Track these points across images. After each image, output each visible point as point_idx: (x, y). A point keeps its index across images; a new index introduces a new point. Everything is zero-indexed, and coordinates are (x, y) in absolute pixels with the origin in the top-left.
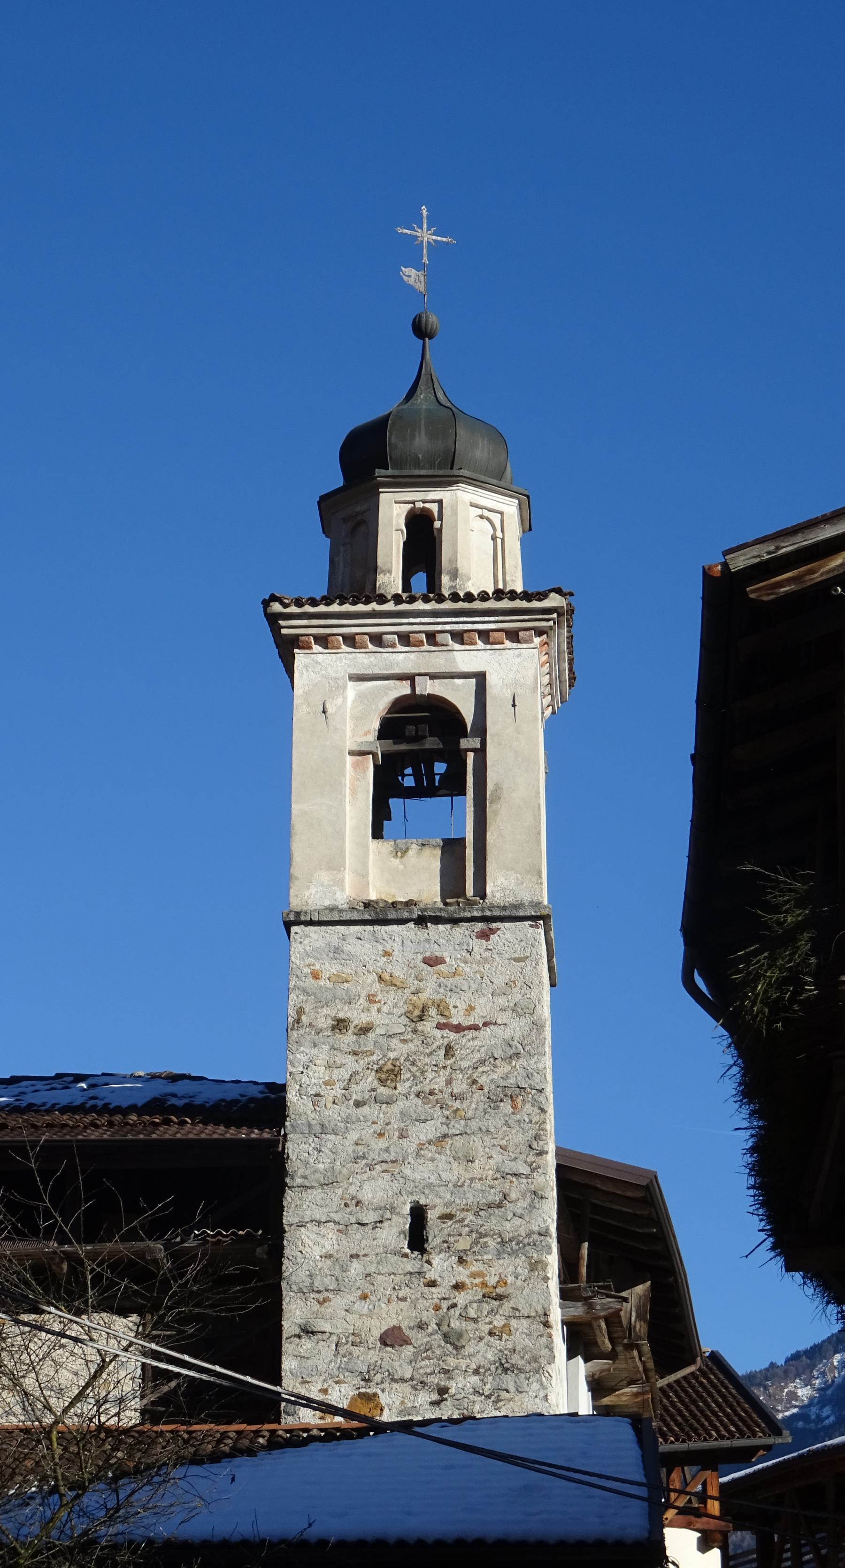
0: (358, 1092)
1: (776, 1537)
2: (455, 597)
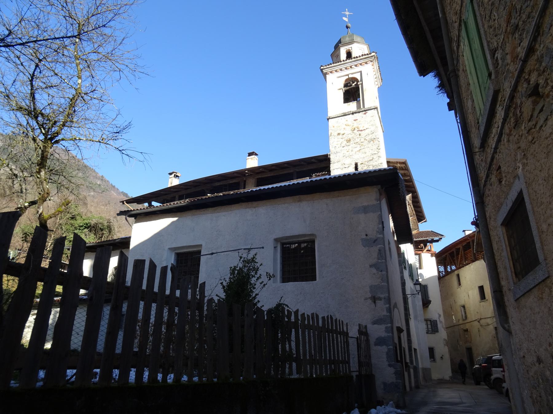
0: (343, 145)
2: (354, 58)
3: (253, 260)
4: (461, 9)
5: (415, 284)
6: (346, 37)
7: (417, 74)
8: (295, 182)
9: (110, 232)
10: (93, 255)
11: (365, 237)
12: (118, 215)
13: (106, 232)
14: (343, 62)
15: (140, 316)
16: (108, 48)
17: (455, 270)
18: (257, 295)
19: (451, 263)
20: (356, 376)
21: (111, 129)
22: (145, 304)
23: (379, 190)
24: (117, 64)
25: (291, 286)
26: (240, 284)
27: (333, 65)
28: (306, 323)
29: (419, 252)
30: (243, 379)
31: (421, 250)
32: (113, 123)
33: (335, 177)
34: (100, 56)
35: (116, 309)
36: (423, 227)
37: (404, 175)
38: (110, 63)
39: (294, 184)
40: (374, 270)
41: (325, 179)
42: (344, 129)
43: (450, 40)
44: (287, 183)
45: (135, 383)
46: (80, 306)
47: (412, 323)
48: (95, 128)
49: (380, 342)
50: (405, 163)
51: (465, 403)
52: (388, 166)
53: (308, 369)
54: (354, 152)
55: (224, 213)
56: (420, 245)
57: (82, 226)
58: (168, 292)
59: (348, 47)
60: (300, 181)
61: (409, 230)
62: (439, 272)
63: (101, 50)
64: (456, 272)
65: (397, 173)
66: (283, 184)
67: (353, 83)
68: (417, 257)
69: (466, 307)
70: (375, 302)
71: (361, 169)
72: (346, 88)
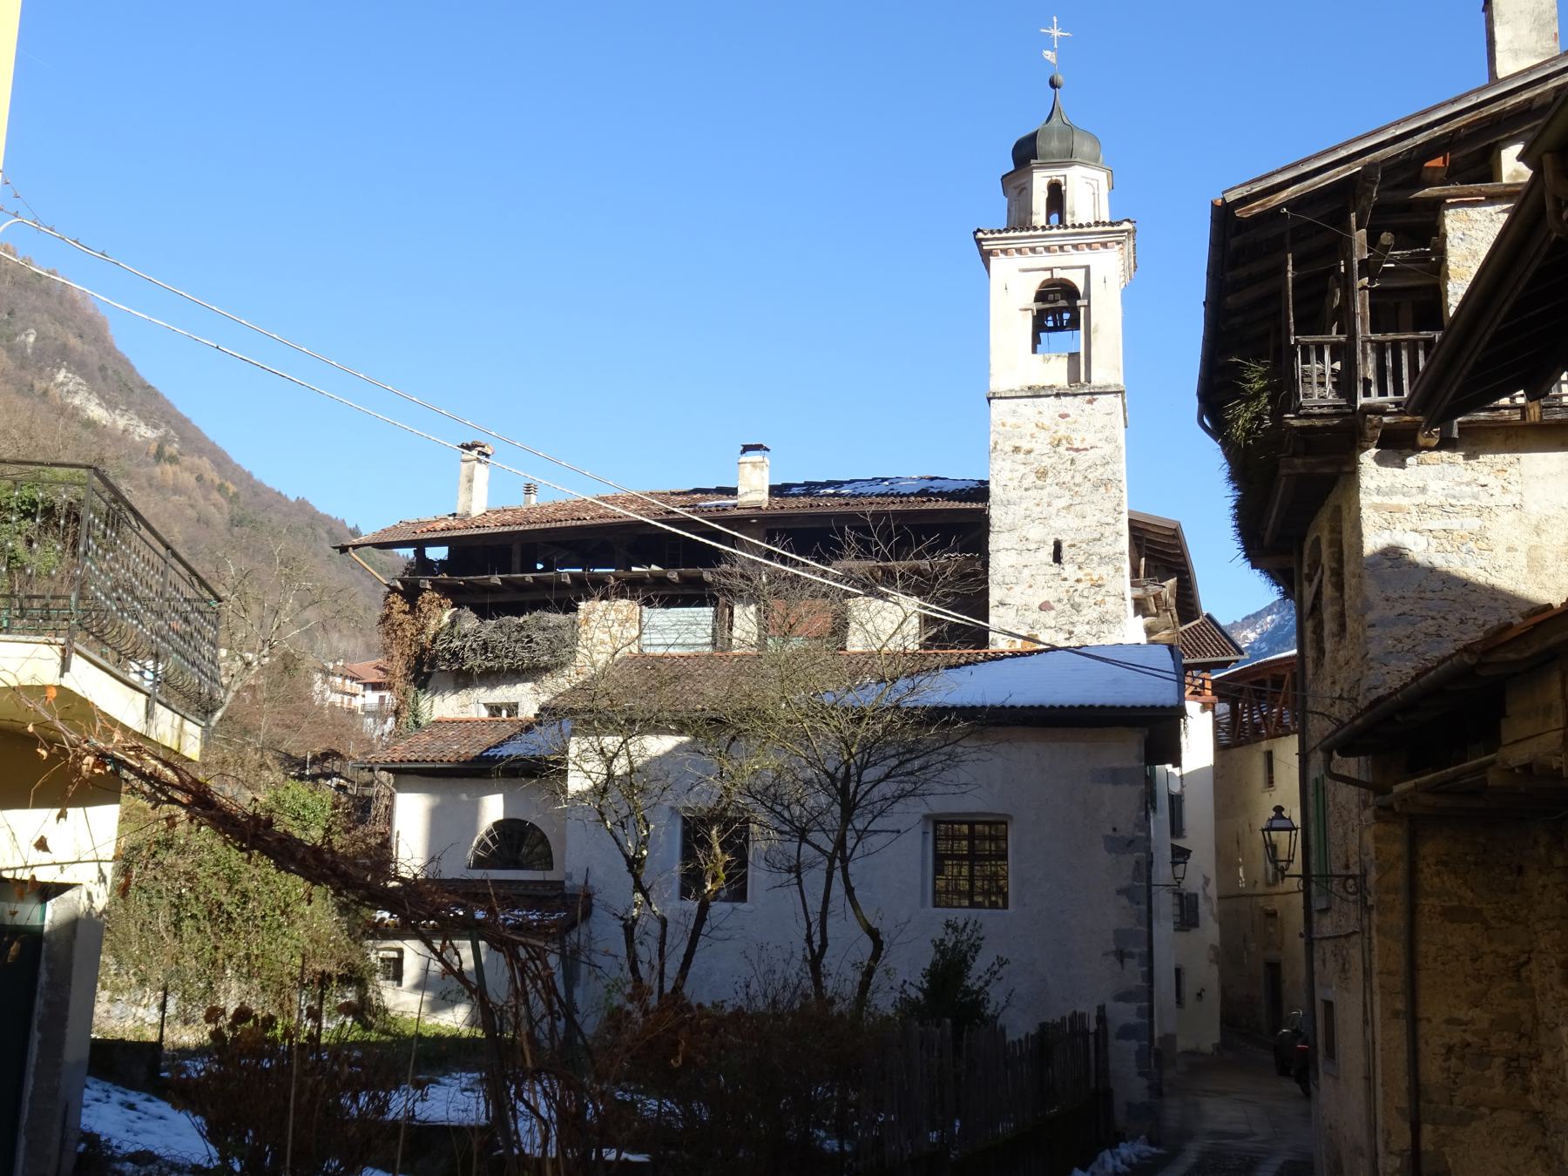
0: (1026, 484)
2: (1074, 226)
11: (1110, 833)
27: (1011, 234)
40: (1124, 901)
42: (1032, 436)
49: (1126, 1032)
54: (1053, 510)
59: (1056, 174)
72: (1041, 305)
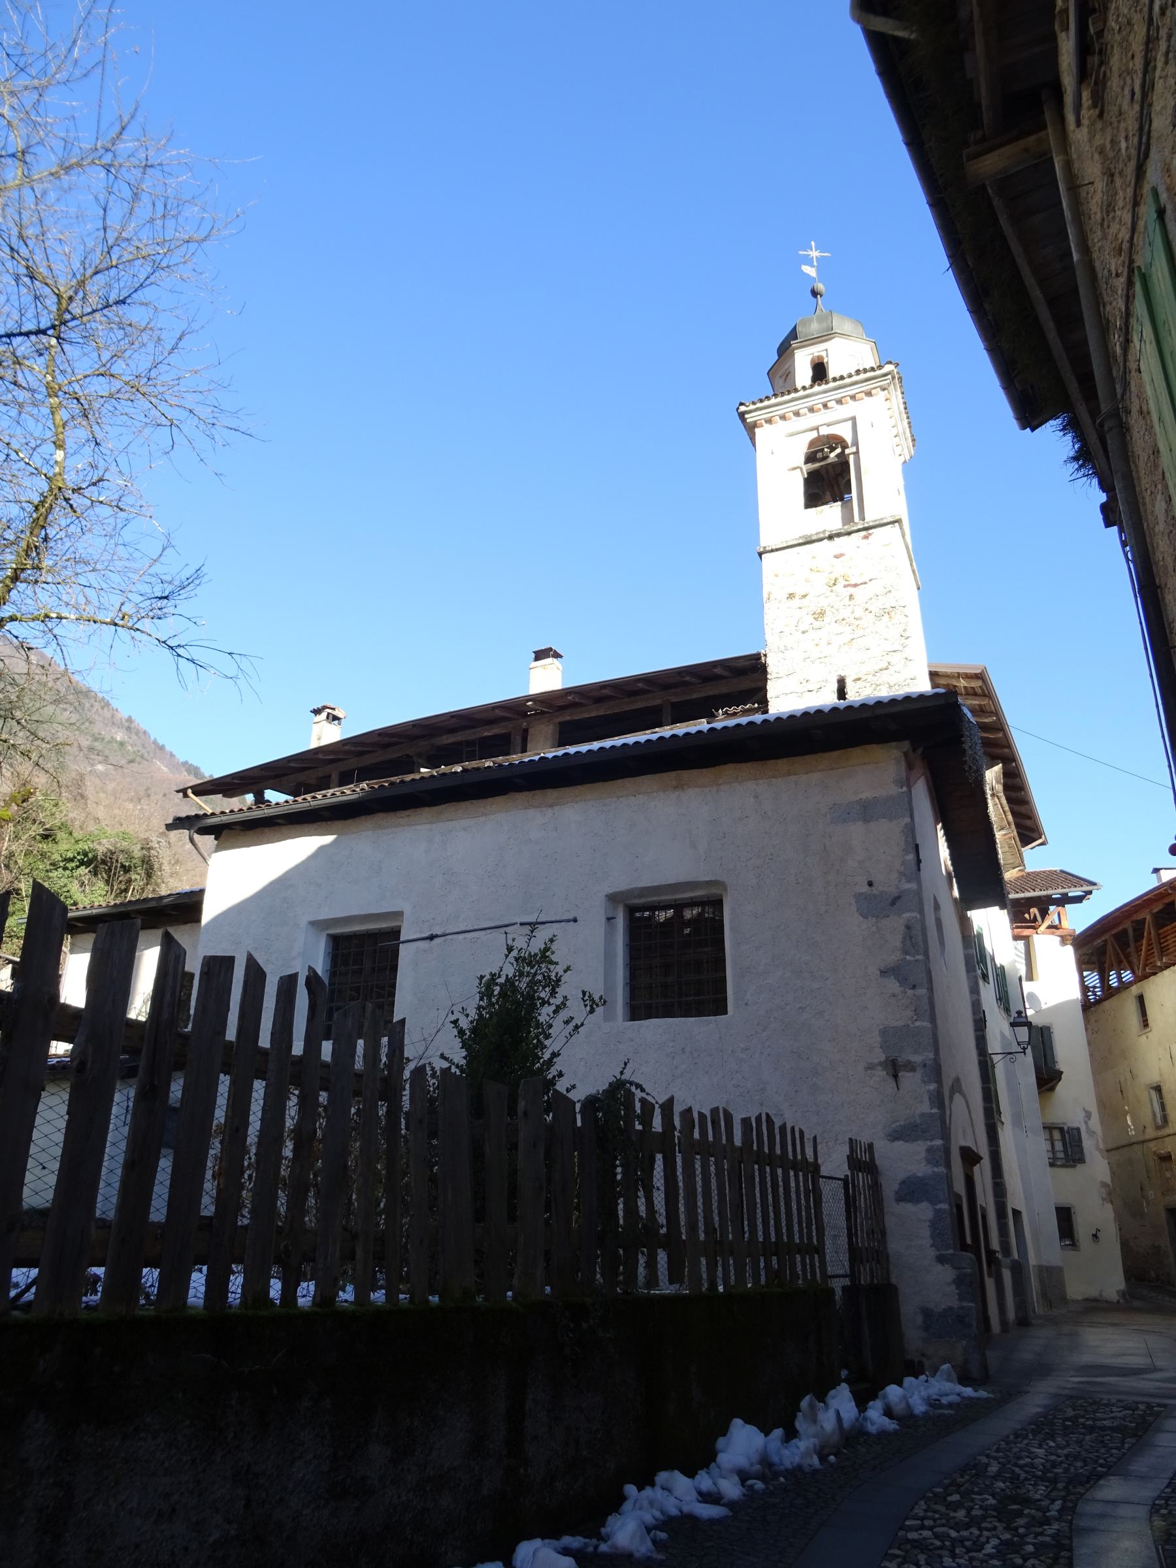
0: (802, 627)
1: (621, 1252)
2: (835, 380)
3: (544, 956)
4: (1132, 238)
5: (1013, 1025)
6: (810, 321)
7: (1014, 424)
8: (666, 732)
9: (149, 875)
10: (89, 939)
11: (865, 889)
12: (169, 827)
13: (137, 877)
14: (801, 393)
15: (220, 1115)
16: (141, 362)
17: (1131, 984)
18: (555, 1055)
19: (1120, 962)
20: (844, 1288)
21: (146, 589)
22: (233, 1083)
23: (906, 754)
24: (163, 407)
25: (655, 1028)
26: (508, 1025)
27: (773, 401)
28: (696, 1135)
29: (1026, 932)
30: (514, 1298)
31: (1033, 924)
32: (152, 571)
33: (778, 719)
34: (117, 384)
35: (151, 1096)
36: (1036, 859)
37: (979, 711)
38: (142, 403)
39: (661, 738)
40: (893, 985)
41: (751, 723)
43: (1104, 329)
44: (642, 737)
45: (205, 1307)
46: (51, 1088)
47: (1006, 1135)
48: (104, 586)
49: (912, 1190)
50: (981, 677)
51: (1161, 1370)
52: (934, 685)
53: (704, 1269)
55: (464, 823)
56: (1027, 913)
57: (71, 860)
58: (298, 1049)
59: (816, 350)
60: (680, 729)
61: (995, 869)
62: (1085, 989)
63: (118, 367)
64: (1135, 990)
65: (957, 707)
66: (630, 739)
67: (832, 449)
68: (1021, 944)
69: (1164, 1089)
70: (896, 1076)
71: (855, 695)
72: (811, 466)
